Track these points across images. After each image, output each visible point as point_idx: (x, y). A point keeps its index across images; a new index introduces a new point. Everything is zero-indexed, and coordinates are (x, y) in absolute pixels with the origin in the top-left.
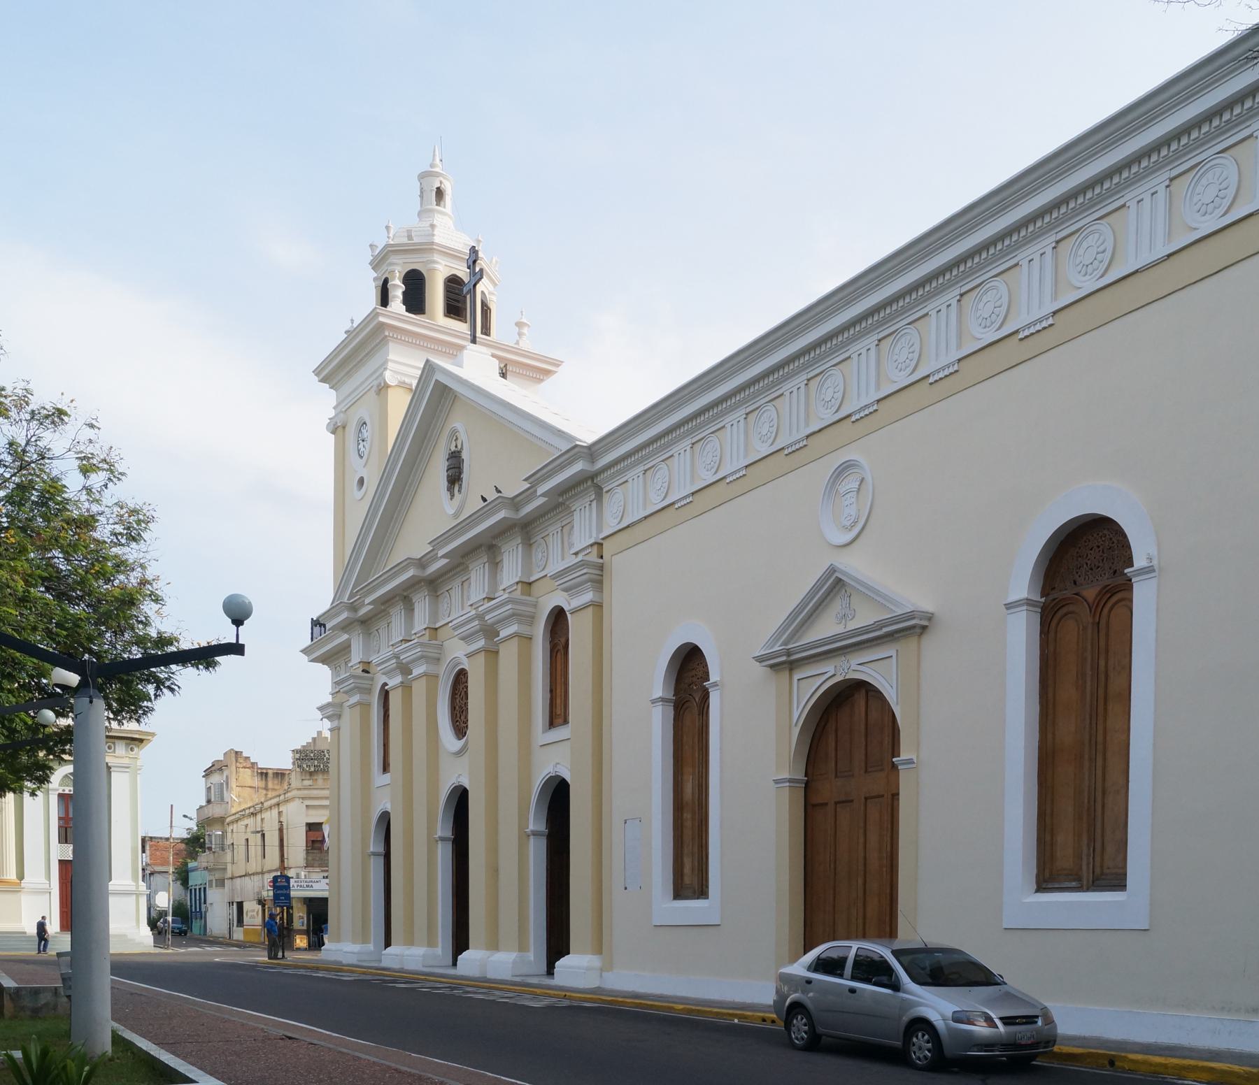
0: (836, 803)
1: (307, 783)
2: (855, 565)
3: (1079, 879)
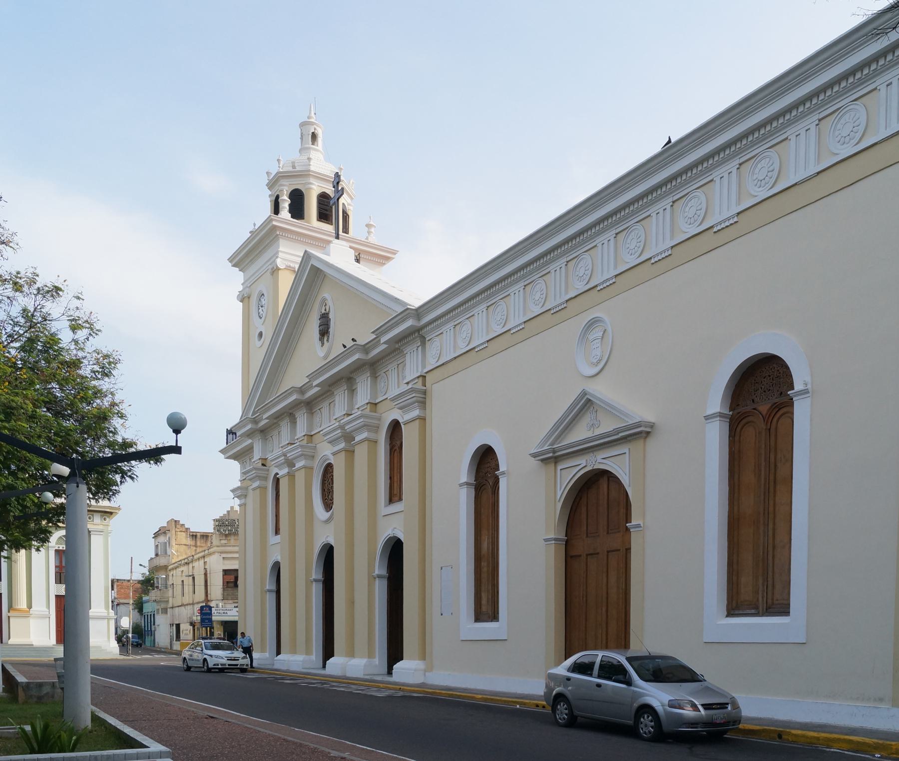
0: (587, 555)
1: (224, 542)
2: (600, 390)
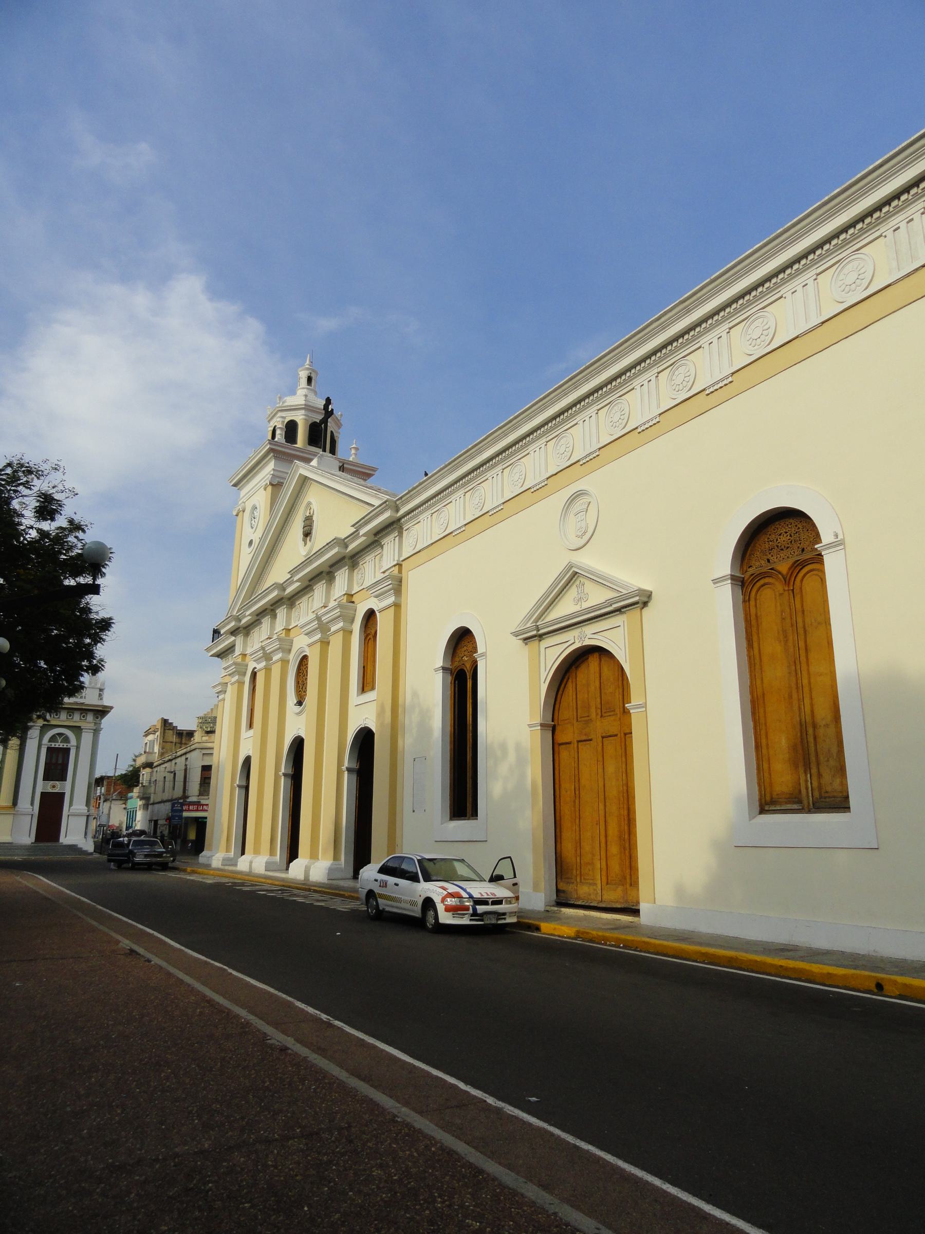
0: (578, 742)
2: (586, 560)
3: (800, 802)
